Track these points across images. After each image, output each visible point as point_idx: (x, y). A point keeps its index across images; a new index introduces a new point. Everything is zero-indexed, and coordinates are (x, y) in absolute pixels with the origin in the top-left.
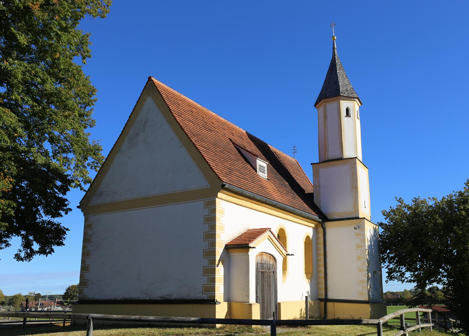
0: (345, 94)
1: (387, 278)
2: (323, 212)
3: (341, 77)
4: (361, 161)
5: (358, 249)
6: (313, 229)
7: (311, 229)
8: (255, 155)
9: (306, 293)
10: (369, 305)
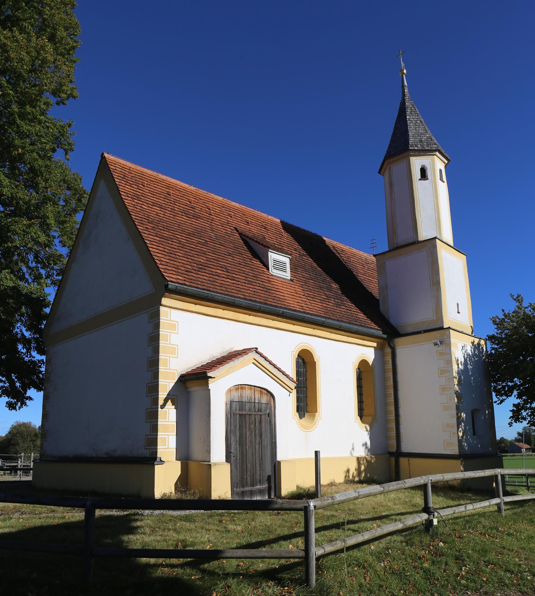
0: (417, 147)
1: (511, 419)
2: (393, 324)
3: (413, 124)
4: (452, 245)
5: (441, 376)
6: (374, 349)
7: (372, 350)
8: (265, 246)
9: (361, 444)
10: (459, 462)
